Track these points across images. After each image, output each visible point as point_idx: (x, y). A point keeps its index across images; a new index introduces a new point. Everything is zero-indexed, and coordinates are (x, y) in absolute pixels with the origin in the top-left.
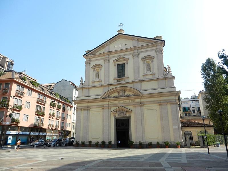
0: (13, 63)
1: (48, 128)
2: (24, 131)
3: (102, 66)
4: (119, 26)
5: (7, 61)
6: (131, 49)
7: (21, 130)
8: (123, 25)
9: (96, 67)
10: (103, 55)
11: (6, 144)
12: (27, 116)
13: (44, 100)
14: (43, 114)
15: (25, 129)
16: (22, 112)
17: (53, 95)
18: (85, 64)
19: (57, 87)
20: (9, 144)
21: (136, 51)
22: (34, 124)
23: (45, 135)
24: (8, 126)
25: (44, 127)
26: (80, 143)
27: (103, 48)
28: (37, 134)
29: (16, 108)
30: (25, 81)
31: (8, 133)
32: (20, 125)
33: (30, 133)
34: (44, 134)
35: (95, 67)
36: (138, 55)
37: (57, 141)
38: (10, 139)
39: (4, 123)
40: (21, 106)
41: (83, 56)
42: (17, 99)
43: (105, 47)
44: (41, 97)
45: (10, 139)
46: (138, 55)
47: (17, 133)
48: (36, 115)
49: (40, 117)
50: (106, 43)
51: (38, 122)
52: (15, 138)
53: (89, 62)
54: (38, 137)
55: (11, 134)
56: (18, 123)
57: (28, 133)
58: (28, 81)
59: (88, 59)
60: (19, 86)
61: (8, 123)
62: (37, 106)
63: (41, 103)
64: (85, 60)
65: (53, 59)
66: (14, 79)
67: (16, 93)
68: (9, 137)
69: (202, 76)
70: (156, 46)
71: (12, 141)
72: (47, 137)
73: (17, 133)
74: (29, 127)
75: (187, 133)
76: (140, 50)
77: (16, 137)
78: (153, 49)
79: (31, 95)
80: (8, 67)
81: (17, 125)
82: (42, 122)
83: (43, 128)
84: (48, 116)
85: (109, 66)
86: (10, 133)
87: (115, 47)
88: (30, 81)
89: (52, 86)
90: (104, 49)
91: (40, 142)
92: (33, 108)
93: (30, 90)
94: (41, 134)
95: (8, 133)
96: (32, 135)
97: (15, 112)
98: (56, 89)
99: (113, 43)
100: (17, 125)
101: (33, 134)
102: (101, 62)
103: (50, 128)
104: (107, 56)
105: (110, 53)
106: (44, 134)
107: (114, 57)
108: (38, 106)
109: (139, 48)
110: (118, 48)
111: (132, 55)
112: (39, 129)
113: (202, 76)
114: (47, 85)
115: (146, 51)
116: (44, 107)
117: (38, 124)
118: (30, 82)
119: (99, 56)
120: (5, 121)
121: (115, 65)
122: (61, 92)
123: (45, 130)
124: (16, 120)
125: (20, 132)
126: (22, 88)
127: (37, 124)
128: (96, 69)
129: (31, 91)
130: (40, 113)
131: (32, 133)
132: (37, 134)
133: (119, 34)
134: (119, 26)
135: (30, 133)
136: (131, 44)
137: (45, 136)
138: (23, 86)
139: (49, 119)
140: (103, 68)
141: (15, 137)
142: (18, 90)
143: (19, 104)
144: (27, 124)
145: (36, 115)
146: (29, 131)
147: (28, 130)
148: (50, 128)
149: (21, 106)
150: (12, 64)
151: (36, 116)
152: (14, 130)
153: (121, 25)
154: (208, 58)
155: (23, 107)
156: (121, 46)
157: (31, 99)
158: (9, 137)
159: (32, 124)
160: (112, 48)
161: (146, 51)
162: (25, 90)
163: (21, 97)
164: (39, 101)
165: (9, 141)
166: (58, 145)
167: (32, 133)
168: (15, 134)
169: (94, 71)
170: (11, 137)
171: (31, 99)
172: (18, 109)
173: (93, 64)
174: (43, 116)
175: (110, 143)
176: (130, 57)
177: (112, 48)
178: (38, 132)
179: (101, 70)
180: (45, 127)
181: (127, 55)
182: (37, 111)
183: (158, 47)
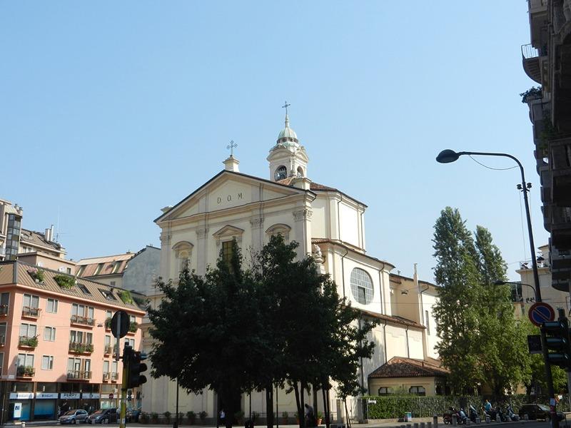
0: (21, 214)
1: (105, 382)
2: (46, 391)
3: (193, 245)
4: (228, 147)
5: (6, 213)
6: (247, 208)
7: (39, 389)
8: (236, 145)
9: (183, 247)
10: (194, 219)
11: (11, 418)
12: (51, 359)
13: (89, 316)
14: (90, 349)
15: (48, 386)
16: (38, 352)
17: (115, 299)
18: (161, 240)
19: (134, 268)
20: (17, 419)
21: (257, 212)
22: (68, 375)
23: (98, 399)
24: (13, 383)
25: (91, 381)
26: (162, 417)
27: (194, 204)
28: (77, 396)
29: (25, 344)
30: (40, 281)
31: (12, 396)
32: (35, 379)
33: (59, 396)
34: (95, 396)
35: (179, 247)
36: (261, 221)
37: (107, 413)
38: (17, 408)
39: (3, 377)
40: (35, 338)
41: (155, 221)
42: (27, 324)
43: (198, 200)
44: (80, 312)
45: (17, 408)
46: (261, 221)
47: (31, 395)
48: (70, 353)
49: (81, 357)
50: (214, 180)
51: (77, 370)
52: (28, 407)
53: (167, 235)
54: (77, 404)
55: (19, 398)
56: (30, 375)
57: (55, 396)
58: (48, 278)
59: (166, 230)
60: (30, 296)
61: (12, 377)
62: (73, 333)
63: (82, 324)
64: (161, 230)
65: (111, 210)
66: (18, 285)
67: (23, 312)
68: (16, 405)
69: (435, 251)
70: (295, 202)
71: (23, 413)
72: (102, 403)
73: (31, 395)
74: (56, 383)
75: (384, 391)
76: (266, 211)
77: (30, 403)
78: (321, 190)
79: (56, 311)
80: (11, 227)
81: (31, 379)
82: (87, 370)
83: (90, 382)
84: (103, 353)
85: (206, 246)
86: (17, 396)
87: (219, 200)
88: (54, 275)
89: (124, 263)
90: (196, 205)
91: (77, 414)
92: (64, 339)
93: (52, 300)
94: (86, 396)
95: (12, 396)
96: (64, 401)
97: (24, 352)
98: (133, 272)
99: (214, 192)
100: (31, 379)
101: (68, 398)
102: (190, 236)
103: (110, 382)
104: (202, 223)
105: (207, 216)
106: (95, 396)
107: (215, 224)
108: (75, 332)
109: (262, 205)
110: (225, 205)
111: (249, 222)
112: (81, 386)
113: (435, 251)
114: (111, 260)
115: (277, 212)
116: (91, 334)
117: (77, 374)
118: (54, 278)
119: (187, 221)
120: (6, 373)
121: (218, 245)
122: (145, 280)
123: (95, 388)
124: (28, 370)
125: (38, 394)
126: (36, 299)
127: (73, 374)
128: (181, 252)
129: (56, 301)
130: (80, 349)
131: (63, 396)
132: (77, 396)
133: (225, 173)
134: (228, 147)
135: (59, 396)
136: (249, 195)
137: (96, 403)
138: (37, 294)
139: (106, 359)
140: (194, 251)
141: (27, 404)
142: (28, 306)
143: (31, 336)
144: (52, 376)
145: (70, 353)
146: (56, 392)
147: (55, 390)
148: (110, 382)
149: (35, 338)
150: (18, 218)
151: (72, 356)
152: (25, 390)
153: (232, 146)
154: (447, 208)
155: (39, 339)
156: (229, 199)
157: (56, 320)
158: (16, 405)
159: (63, 376)
160: (213, 202)
161: (277, 212)
162: (43, 303)
163: (35, 320)
164: (76, 321)
165: (17, 414)
166: (107, 420)
167: (63, 396)
168: (27, 398)
169: (177, 256)
170: (19, 405)
171: (56, 320)
172: (29, 345)
173: (176, 239)
174: (89, 355)
175: (203, 415)
176: (245, 225)
177: (213, 202)
178: (78, 392)
179: (190, 254)
180: (96, 379)
181: (241, 220)
182: (72, 345)
183: (298, 204)
